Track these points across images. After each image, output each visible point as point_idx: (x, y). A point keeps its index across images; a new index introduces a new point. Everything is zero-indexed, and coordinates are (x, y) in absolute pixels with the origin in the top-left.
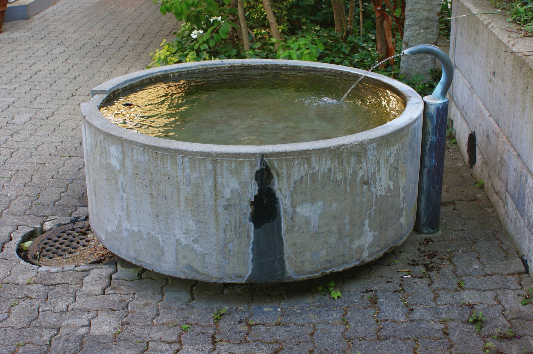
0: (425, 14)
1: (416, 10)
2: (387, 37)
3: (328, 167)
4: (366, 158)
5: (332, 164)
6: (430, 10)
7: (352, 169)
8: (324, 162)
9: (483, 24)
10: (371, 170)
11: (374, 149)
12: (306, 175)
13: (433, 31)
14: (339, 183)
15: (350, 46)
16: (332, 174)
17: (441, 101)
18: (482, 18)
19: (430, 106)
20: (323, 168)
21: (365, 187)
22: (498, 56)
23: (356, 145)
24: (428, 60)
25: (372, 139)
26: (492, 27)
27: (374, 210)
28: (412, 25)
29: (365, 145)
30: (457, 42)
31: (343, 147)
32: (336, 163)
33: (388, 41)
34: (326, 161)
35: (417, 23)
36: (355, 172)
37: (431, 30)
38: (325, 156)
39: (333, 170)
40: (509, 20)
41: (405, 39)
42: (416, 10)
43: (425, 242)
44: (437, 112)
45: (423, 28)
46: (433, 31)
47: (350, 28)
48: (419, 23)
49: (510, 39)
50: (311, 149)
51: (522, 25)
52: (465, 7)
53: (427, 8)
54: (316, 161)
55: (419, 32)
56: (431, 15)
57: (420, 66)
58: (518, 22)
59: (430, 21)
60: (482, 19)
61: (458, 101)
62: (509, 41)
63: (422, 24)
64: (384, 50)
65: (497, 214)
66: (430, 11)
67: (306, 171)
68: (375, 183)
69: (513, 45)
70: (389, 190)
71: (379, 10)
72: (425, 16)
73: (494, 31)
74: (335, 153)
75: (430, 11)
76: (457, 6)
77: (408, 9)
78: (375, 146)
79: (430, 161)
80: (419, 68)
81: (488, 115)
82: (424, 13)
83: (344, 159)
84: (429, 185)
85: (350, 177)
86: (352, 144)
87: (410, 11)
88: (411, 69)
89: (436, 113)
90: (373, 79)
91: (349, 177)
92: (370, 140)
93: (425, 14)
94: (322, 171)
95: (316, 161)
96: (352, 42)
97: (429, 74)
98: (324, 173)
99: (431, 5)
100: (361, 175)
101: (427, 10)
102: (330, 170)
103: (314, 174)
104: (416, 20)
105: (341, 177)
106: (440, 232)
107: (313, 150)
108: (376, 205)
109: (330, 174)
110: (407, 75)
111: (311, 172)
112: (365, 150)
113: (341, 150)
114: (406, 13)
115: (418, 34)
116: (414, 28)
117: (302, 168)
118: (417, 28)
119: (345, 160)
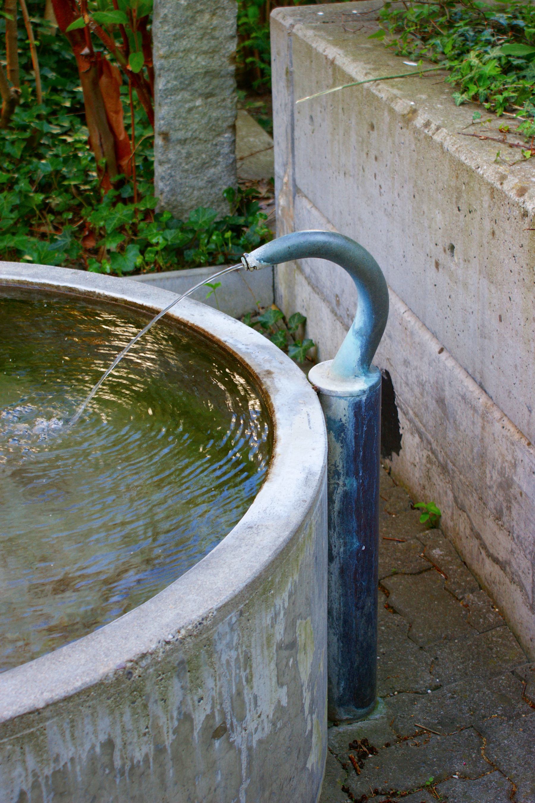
0: (203, 61)
1: (181, 55)
2: (112, 115)
3: (103, 737)
4: (212, 665)
5: (113, 723)
6: (214, 52)
7: (175, 714)
8: (89, 728)
9: (391, 111)
10: (230, 688)
11: (232, 629)
12: (36, 785)
13: (224, 100)
14: (142, 769)
15: (24, 140)
16: (117, 754)
17: (360, 385)
18: (384, 91)
19: (334, 399)
20: (87, 747)
21: (217, 744)
22: (463, 207)
23: (182, 641)
24: (219, 167)
25: (225, 605)
26: (427, 125)
27: (246, 792)
28: (174, 91)
29: (208, 629)
30: (296, 134)
31: (144, 663)
32: (127, 717)
33: (115, 125)
34: (94, 724)
35: (186, 83)
36: (186, 718)
37: (219, 98)
38: (89, 712)
39: (118, 742)
40: (459, 97)
41: (159, 124)
42: (181, 55)
43: (353, 754)
44: (356, 415)
45: (200, 95)
46: (224, 100)
47: (17, 92)
48: (189, 85)
49: (502, 169)
50: (41, 705)
51: (500, 111)
52: (318, 54)
53: (205, 48)
54: (63, 734)
55: (191, 105)
56: (215, 64)
57: (201, 184)
58: (487, 105)
59: (214, 77)
60: (383, 95)
61: (317, 279)
62: (503, 178)
63: (197, 85)
64: (108, 146)
65: (502, 613)
66: (212, 52)
67: (35, 775)
68: (242, 719)
69: (522, 192)
70: (279, 709)
71: (87, 56)
72: (203, 67)
73: (437, 138)
74: (123, 688)
75: (212, 52)
76: (289, 47)
77: (161, 52)
78: (234, 620)
79: (345, 544)
80: (200, 189)
81: (435, 347)
82: (199, 59)
83: (148, 696)
84: (346, 604)
85: (172, 737)
86: (168, 643)
87: (166, 57)
88: (183, 194)
89: (353, 420)
90: (142, 307)
91: (169, 739)
92: (219, 609)
93: (203, 61)
94: (84, 756)
95: (63, 734)
96: (23, 128)
97: (225, 199)
98: (93, 759)
99: (213, 38)
100: (203, 718)
101: (205, 53)
102: (109, 744)
103: (60, 775)
104: (182, 76)
105: (145, 749)
106: (381, 711)
107: (47, 705)
108: (249, 775)
109: (112, 754)
110: (174, 207)
111: (48, 771)
112: (210, 643)
113: (136, 673)
114: (157, 63)
115: (190, 110)
116: (179, 98)
117: (19, 770)
118: (187, 95)
119: (155, 696)
